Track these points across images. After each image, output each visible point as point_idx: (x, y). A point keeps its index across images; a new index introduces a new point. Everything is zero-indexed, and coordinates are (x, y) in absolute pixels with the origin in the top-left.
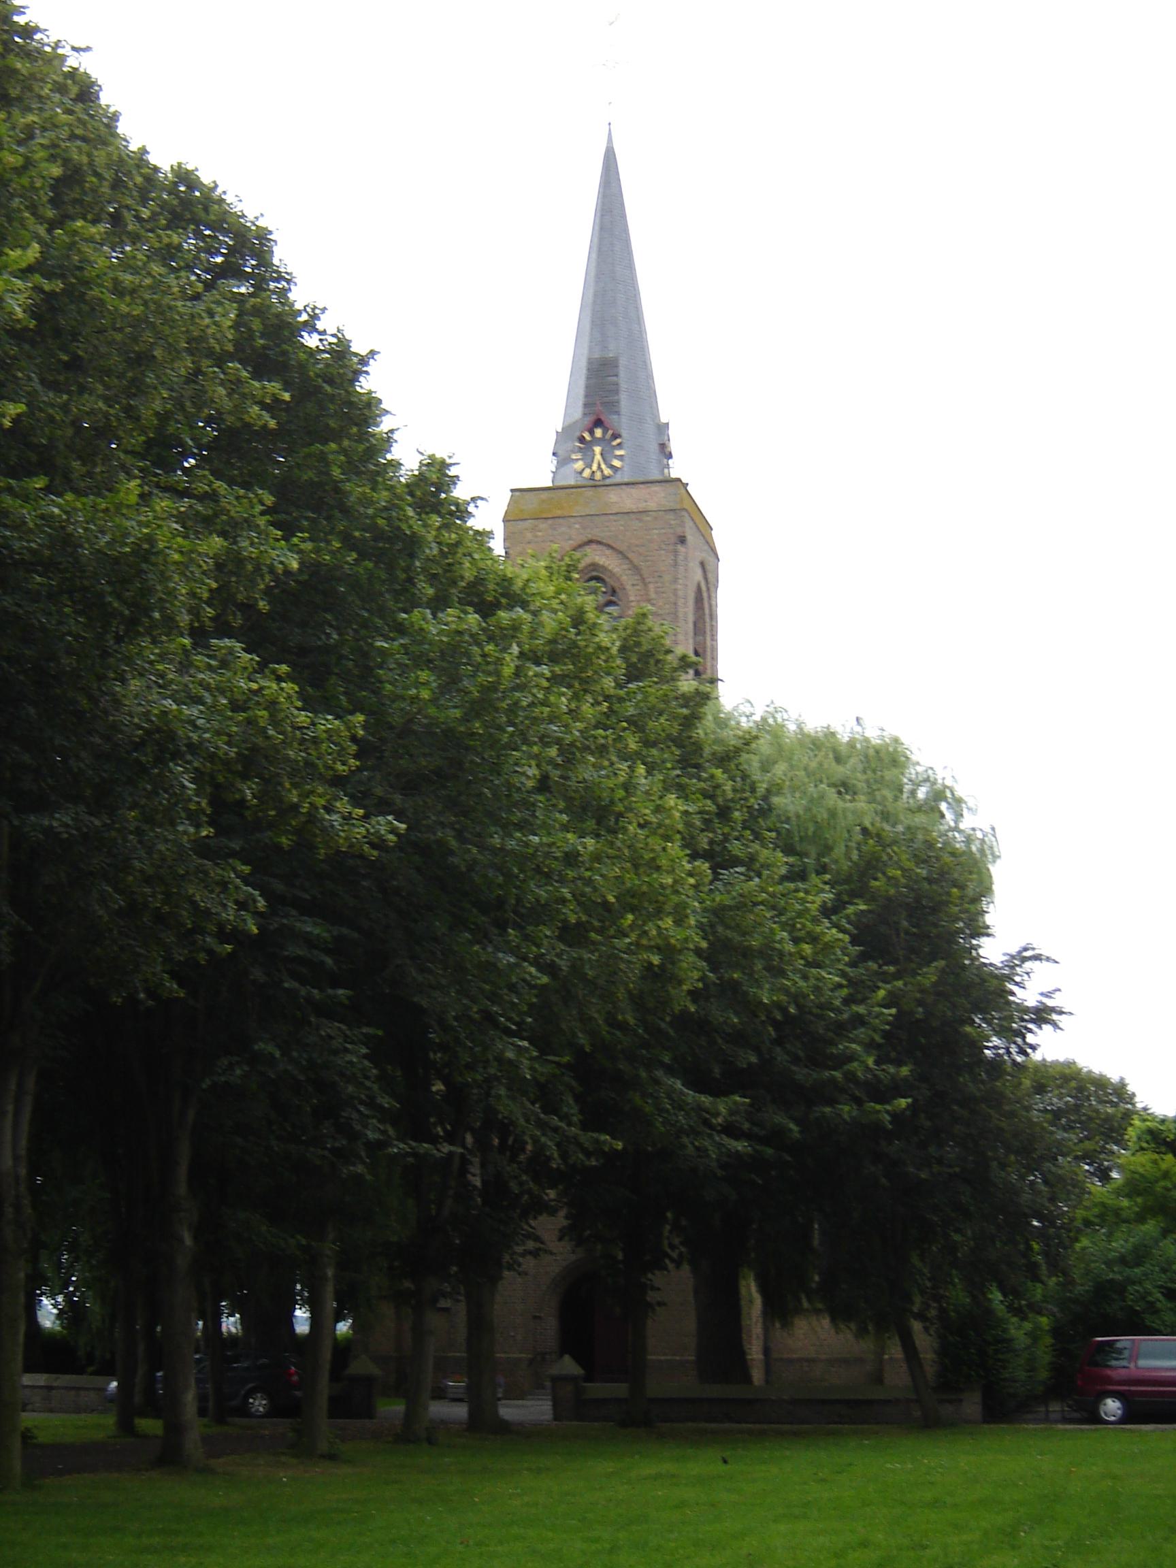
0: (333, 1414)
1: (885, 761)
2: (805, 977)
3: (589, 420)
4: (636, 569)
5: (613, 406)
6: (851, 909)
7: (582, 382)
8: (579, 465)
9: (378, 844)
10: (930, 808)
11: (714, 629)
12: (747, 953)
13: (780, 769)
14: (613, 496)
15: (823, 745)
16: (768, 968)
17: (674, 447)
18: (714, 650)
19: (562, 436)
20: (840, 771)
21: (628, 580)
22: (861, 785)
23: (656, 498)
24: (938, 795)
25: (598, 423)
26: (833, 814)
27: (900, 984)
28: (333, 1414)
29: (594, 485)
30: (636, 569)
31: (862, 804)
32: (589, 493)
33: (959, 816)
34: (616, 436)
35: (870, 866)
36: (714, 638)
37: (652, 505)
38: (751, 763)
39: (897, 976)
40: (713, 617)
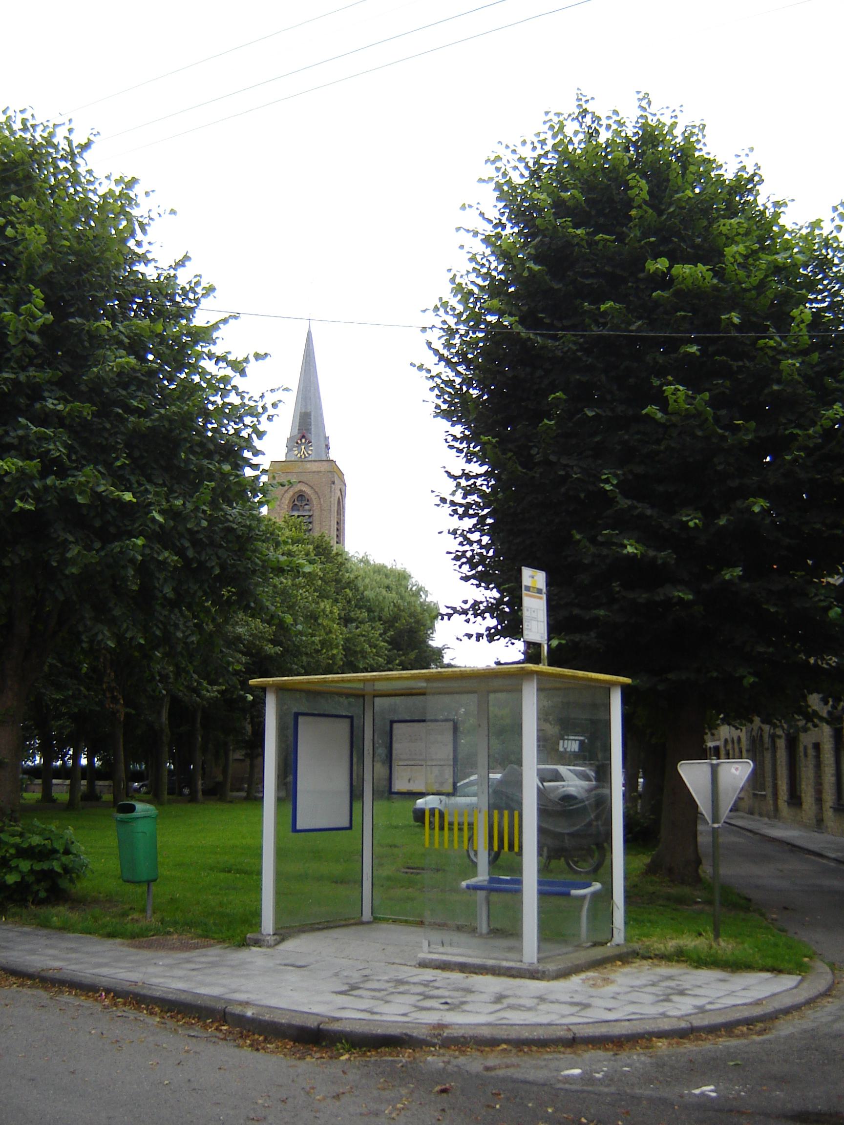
0: (169, 794)
1: (403, 577)
2: (374, 659)
3: (300, 436)
4: (316, 493)
5: (309, 430)
6: (388, 634)
7: (298, 420)
8: (296, 452)
9: (276, 653)
10: (417, 594)
11: (344, 513)
12: (355, 652)
13: (367, 581)
14: (308, 465)
15: (380, 570)
16: (362, 657)
17: (331, 446)
18: (344, 520)
19: (290, 440)
20: (387, 582)
21: (313, 497)
22: (394, 587)
23: (324, 467)
24: (420, 589)
25: (303, 437)
26: (384, 598)
27: (403, 658)
28: (169, 794)
29: (302, 461)
30: (316, 493)
31: (394, 595)
32: (300, 463)
33: (427, 596)
34: (310, 442)
35: (396, 618)
36: (344, 516)
37: (323, 469)
38: (360, 584)
39: (403, 655)
40: (344, 508)
